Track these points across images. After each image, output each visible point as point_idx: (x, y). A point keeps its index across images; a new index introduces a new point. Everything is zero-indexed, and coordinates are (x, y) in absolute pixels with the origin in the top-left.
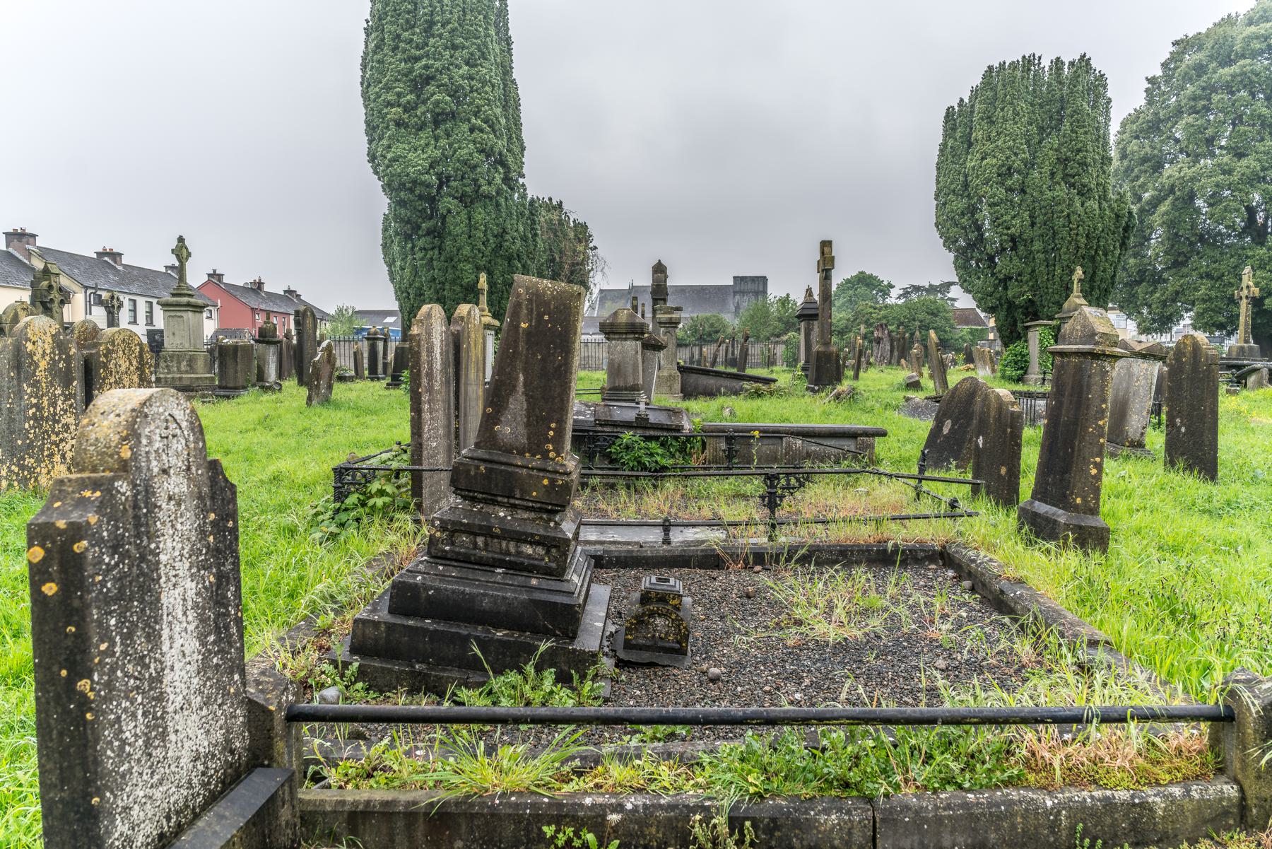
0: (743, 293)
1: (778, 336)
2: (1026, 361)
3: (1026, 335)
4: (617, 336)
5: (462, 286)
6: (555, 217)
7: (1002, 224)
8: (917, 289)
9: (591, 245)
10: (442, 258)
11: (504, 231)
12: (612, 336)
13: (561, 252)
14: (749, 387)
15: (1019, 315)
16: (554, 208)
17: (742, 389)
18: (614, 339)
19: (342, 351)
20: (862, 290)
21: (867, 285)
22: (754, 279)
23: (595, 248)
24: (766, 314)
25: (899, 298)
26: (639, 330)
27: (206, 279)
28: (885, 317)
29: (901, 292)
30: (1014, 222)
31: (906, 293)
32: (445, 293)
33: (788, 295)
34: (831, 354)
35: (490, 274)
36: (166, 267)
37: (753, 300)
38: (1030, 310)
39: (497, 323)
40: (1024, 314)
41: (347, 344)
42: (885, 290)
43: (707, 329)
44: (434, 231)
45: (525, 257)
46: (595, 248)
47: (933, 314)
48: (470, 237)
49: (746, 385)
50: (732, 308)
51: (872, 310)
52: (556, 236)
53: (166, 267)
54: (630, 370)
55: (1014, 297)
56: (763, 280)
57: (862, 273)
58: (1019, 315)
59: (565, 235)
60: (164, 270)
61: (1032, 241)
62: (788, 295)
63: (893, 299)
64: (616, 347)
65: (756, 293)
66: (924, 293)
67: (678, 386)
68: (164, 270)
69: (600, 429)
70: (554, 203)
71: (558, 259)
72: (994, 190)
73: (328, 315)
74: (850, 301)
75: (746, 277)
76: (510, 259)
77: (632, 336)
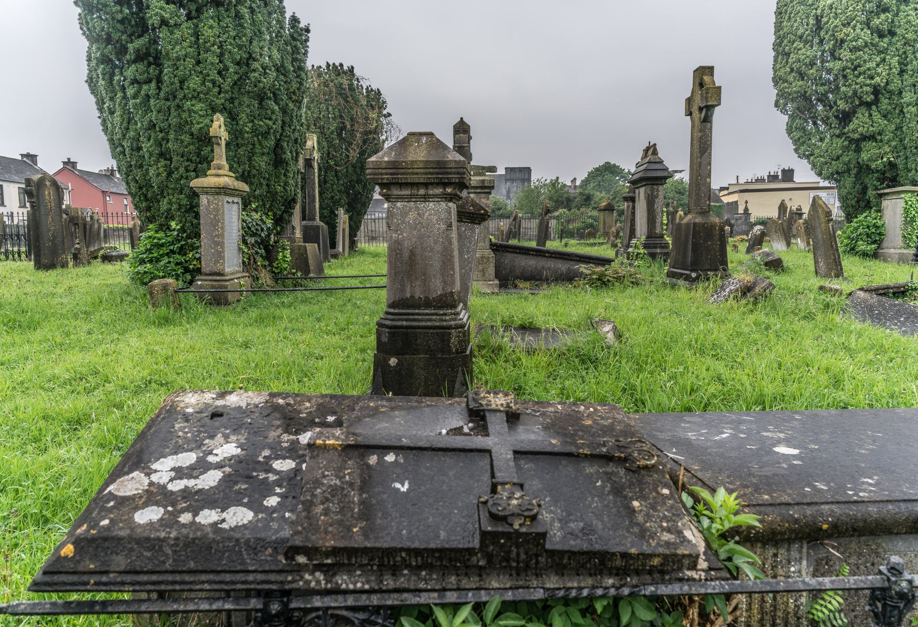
2: (880, 234)
3: (879, 204)
4: (406, 192)
5: (192, 134)
6: (345, 82)
7: (864, 73)
9: (385, 112)
10: (162, 94)
11: (251, 57)
12: (396, 192)
13: (352, 120)
14: (588, 272)
15: (871, 181)
16: (345, 73)
17: (581, 275)
18: (401, 198)
19: (381, 225)
20: (608, 176)
21: (612, 173)
22: (521, 170)
23: (389, 115)
26: (455, 178)
27: (61, 166)
30: (879, 70)
32: (170, 145)
33: (558, 178)
34: (713, 226)
35: (232, 118)
36: (22, 155)
38: (887, 175)
39: (246, 188)
40: (878, 179)
45: (285, 97)
46: (389, 115)
47: (680, 193)
48: (198, 63)
49: (583, 268)
50: (504, 192)
52: (347, 102)
53: (22, 155)
54: (436, 264)
55: (869, 160)
56: (528, 170)
58: (871, 181)
59: (357, 101)
60: (20, 158)
61: (900, 93)
62: (558, 178)
64: (404, 214)
67: (491, 271)
68: (20, 158)
69: (316, 580)
70: (345, 68)
71: (349, 127)
72: (858, 31)
74: (599, 185)
75: (515, 168)
76: (261, 98)
77: (438, 191)
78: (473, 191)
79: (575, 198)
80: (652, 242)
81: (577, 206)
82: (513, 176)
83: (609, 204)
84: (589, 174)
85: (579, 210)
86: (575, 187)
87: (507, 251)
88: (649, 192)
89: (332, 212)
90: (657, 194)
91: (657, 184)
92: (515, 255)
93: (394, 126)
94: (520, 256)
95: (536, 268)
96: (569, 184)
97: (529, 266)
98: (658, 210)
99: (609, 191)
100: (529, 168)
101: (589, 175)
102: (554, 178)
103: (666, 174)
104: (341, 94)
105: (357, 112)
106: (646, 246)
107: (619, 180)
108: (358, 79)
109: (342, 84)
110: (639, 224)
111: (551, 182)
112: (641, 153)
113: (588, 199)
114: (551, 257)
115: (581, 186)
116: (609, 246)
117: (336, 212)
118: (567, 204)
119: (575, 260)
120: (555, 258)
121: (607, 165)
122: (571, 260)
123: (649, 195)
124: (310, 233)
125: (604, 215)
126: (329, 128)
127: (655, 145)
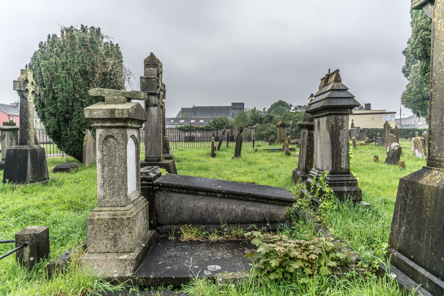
0: (235, 109)
1: (251, 125)
20: (281, 107)
21: (283, 105)
22: (239, 104)
24: (245, 117)
25: (293, 110)
28: (298, 117)
29: (294, 108)
31: (296, 109)
33: (255, 108)
37: (239, 111)
42: (289, 107)
43: (220, 123)
44: (105, 74)
50: (231, 114)
51: (292, 114)
56: (243, 104)
59: (96, 51)
62: (255, 108)
63: (292, 110)
65: (240, 109)
66: (303, 108)
73: (285, 269)
74: (276, 111)
75: (236, 103)
79: (264, 118)
80: (337, 179)
82: (235, 107)
83: (283, 123)
84: (272, 106)
85: (266, 124)
86: (265, 112)
87: (172, 192)
88: (333, 123)
89: (80, 132)
90: (342, 125)
93: (127, 70)
96: (262, 111)
97: (199, 208)
98: (344, 143)
100: (243, 103)
101: (271, 106)
102: (254, 108)
103: (351, 103)
104: (83, 45)
105: (97, 59)
106: (331, 185)
107: (286, 109)
108: (102, 37)
109: (84, 38)
110: (319, 155)
111: (252, 110)
114: (223, 197)
115: (268, 112)
117: (84, 132)
118: (260, 121)
119: (251, 201)
120: (229, 198)
121: (280, 102)
122: (247, 200)
123: (332, 126)
124: (19, 156)
126: (74, 71)
127: (338, 71)
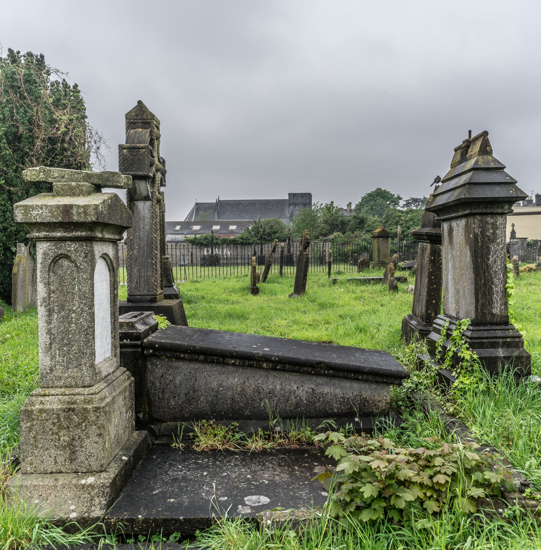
0: (295, 205)
8: (415, 200)
20: (380, 201)
22: (303, 195)
24: (314, 219)
25: (403, 207)
28: (411, 219)
29: (405, 203)
31: (408, 204)
33: (332, 202)
37: (302, 209)
41: (178, 268)
42: (396, 201)
43: (268, 231)
50: (288, 214)
51: (400, 214)
56: (309, 196)
57: (379, 189)
59: (37, 98)
62: (332, 202)
63: (401, 207)
65: (305, 205)
74: (372, 209)
75: (297, 194)
78: (42, 234)
79: (349, 221)
80: (486, 334)
81: (351, 229)
83: (383, 231)
85: (353, 232)
86: (351, 210)
87: (178, 359)
90: (494, 233)
91: (492, 214)
92: (197, 366)
94: (208, 367)
95: (243, 392)
96: (345, 208)
97: (228, 389)
99: (380, 215)
100: (310, 194)
101: (362, 200)
102: (329, 203)
103: (511, 193)
104: (12, 87)
107: (390, 204)
110: (451, 290)
112: (450, 156)
113: (361, 223)
114: (274, 369)
115: (355, 210)
116: (386, 286)
117: (13, 249)
118: (342, 227)
119: (325, 375)
120: (284, 370)
122: (318, 375)
123: (476, 236)
125: (378, 242)
127: (486, 133)
